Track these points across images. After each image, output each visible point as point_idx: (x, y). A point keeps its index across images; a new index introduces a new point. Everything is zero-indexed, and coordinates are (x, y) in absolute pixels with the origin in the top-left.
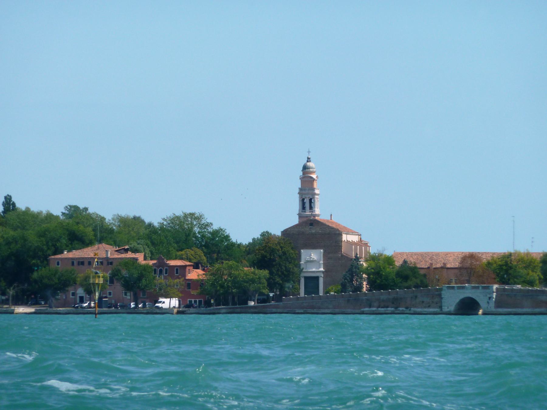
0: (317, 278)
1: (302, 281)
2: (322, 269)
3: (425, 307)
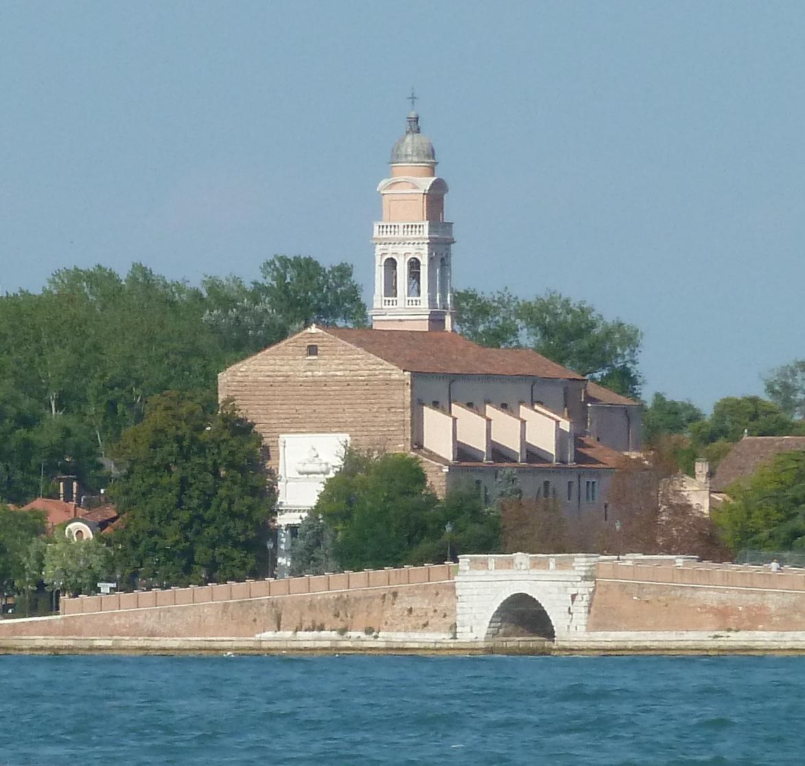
3: (415, 628)
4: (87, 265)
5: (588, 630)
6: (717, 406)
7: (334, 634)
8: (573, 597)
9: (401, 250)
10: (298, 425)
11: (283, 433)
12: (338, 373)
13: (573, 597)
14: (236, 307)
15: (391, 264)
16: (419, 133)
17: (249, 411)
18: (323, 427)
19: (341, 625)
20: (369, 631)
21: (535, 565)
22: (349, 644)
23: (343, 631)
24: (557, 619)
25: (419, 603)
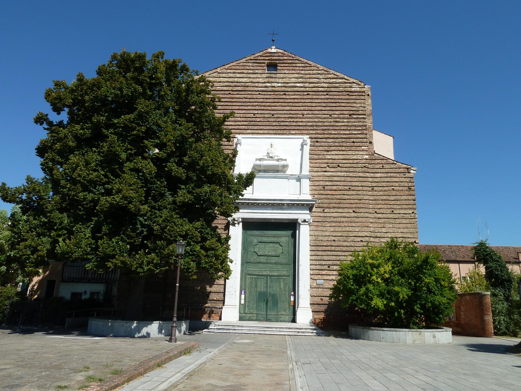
0: (292, 226)
1: (236, 233)
2: (306, 195)
10: (255, 127)
11: (239, 134)
12: (298, 85)
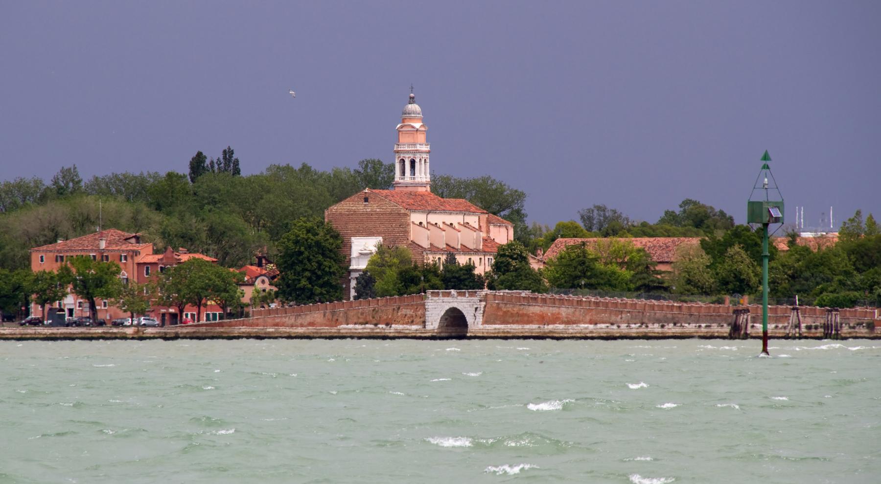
3: (407, 324)
4: (283, 164)
5: (486, 322)
6: (559, 225)
7: (372, 326)
8: (476, 309)
9: (407, 156)
13: (476, 309)
14: (713, 239)
15: (403, 161)
16: (782, 203)
17: (337, 226)
18: (369, 233)
19: (375, 322)
20: (387, 324)
21: (460, 294)
22: (378, 330)
23: (376, 325)
24: (469, 319)
25: (410, 312)
